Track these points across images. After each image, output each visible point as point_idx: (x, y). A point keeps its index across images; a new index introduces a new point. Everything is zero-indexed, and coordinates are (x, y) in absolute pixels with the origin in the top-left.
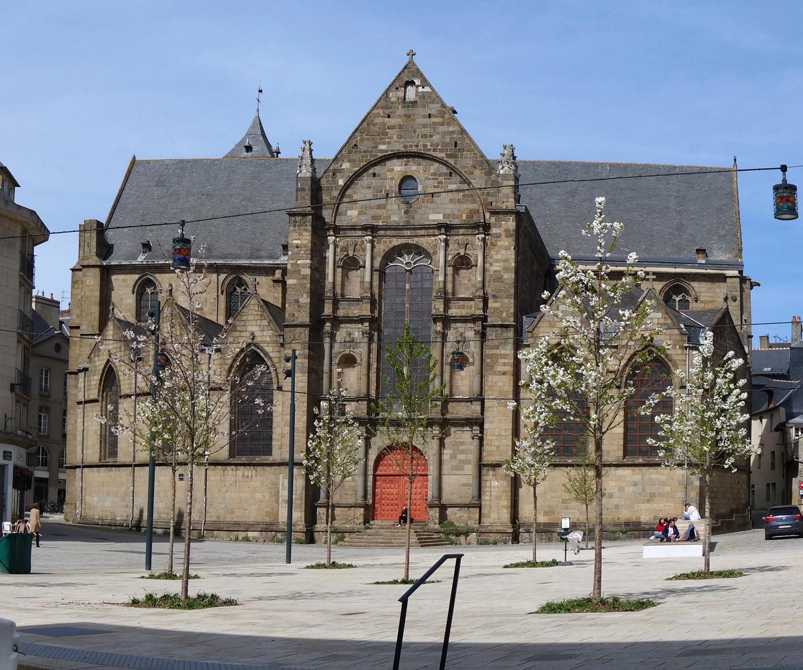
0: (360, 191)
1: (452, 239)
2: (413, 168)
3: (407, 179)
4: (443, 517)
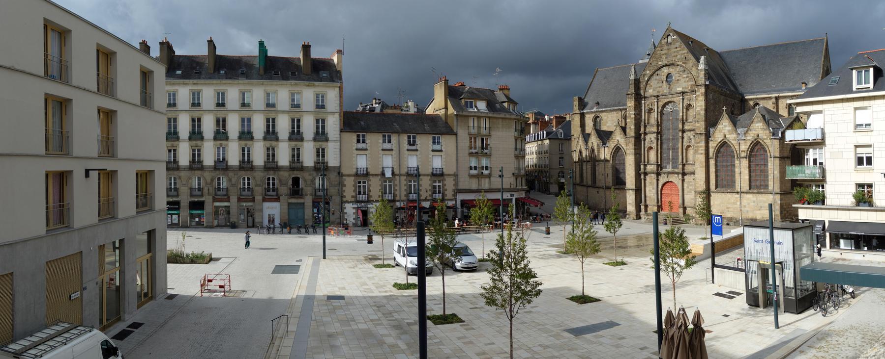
0: (653, 82)
1: (686, 97)
2: (671, 70)
3: (669, 76)
4: (684, 212)
